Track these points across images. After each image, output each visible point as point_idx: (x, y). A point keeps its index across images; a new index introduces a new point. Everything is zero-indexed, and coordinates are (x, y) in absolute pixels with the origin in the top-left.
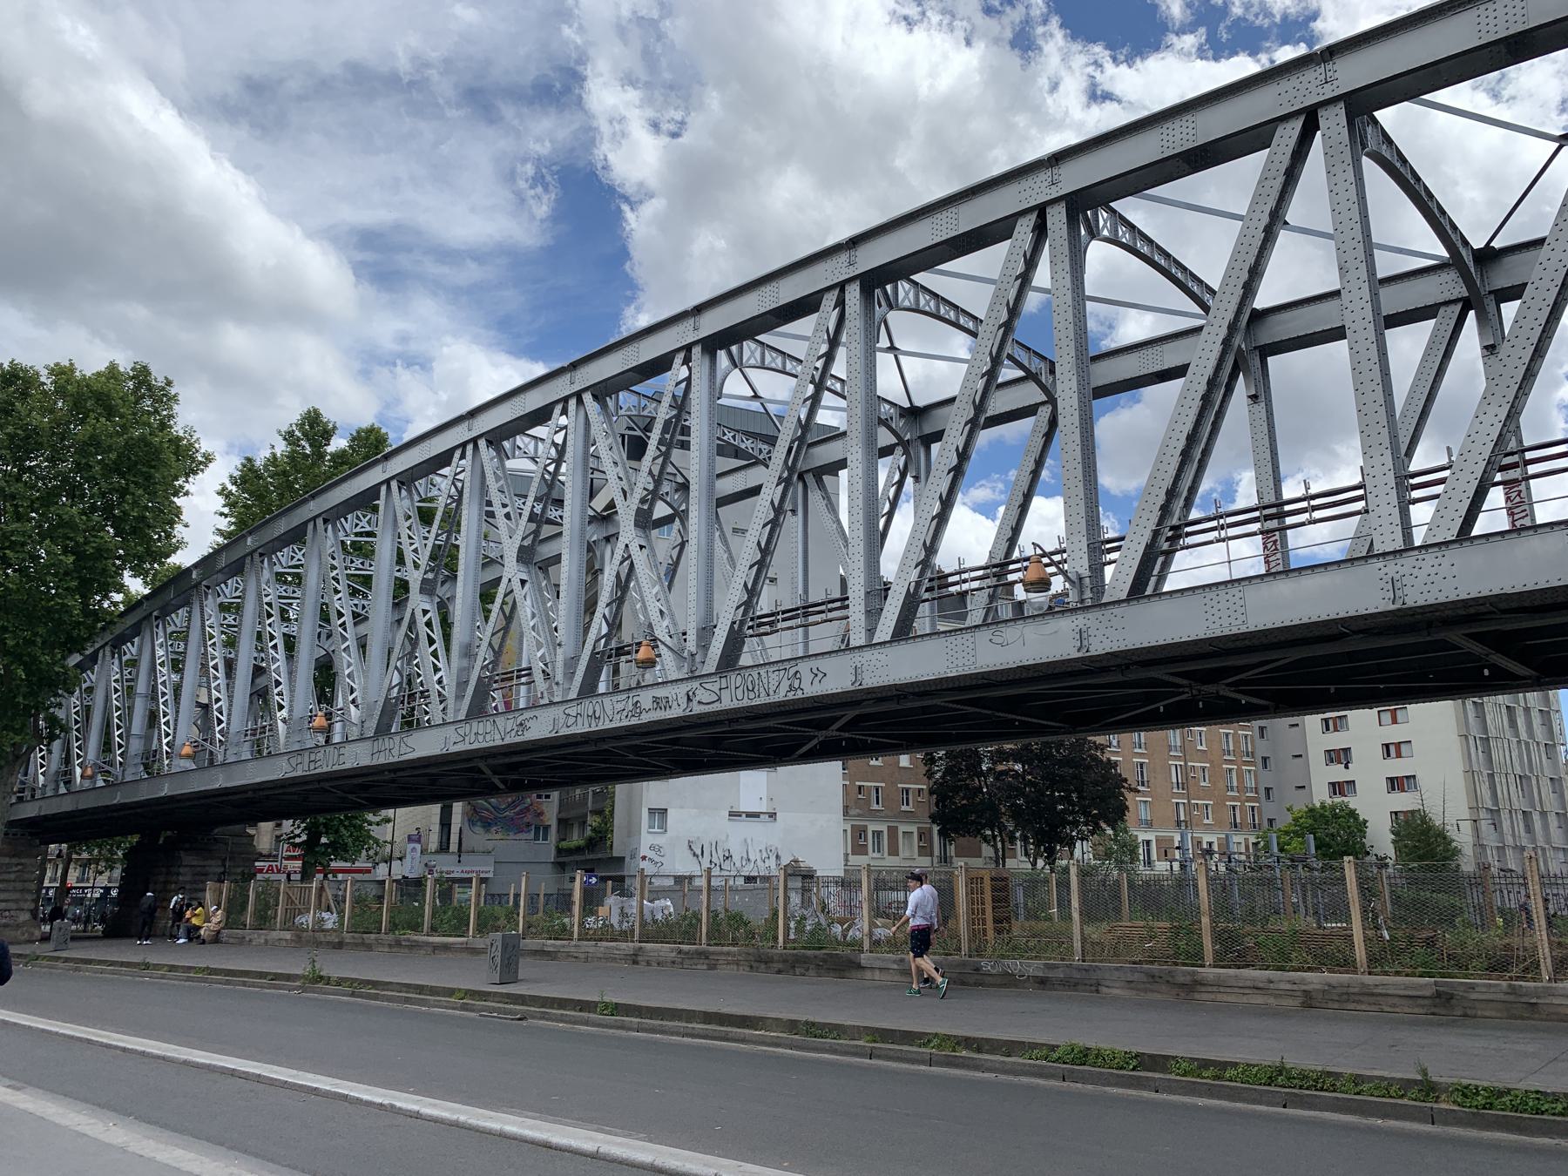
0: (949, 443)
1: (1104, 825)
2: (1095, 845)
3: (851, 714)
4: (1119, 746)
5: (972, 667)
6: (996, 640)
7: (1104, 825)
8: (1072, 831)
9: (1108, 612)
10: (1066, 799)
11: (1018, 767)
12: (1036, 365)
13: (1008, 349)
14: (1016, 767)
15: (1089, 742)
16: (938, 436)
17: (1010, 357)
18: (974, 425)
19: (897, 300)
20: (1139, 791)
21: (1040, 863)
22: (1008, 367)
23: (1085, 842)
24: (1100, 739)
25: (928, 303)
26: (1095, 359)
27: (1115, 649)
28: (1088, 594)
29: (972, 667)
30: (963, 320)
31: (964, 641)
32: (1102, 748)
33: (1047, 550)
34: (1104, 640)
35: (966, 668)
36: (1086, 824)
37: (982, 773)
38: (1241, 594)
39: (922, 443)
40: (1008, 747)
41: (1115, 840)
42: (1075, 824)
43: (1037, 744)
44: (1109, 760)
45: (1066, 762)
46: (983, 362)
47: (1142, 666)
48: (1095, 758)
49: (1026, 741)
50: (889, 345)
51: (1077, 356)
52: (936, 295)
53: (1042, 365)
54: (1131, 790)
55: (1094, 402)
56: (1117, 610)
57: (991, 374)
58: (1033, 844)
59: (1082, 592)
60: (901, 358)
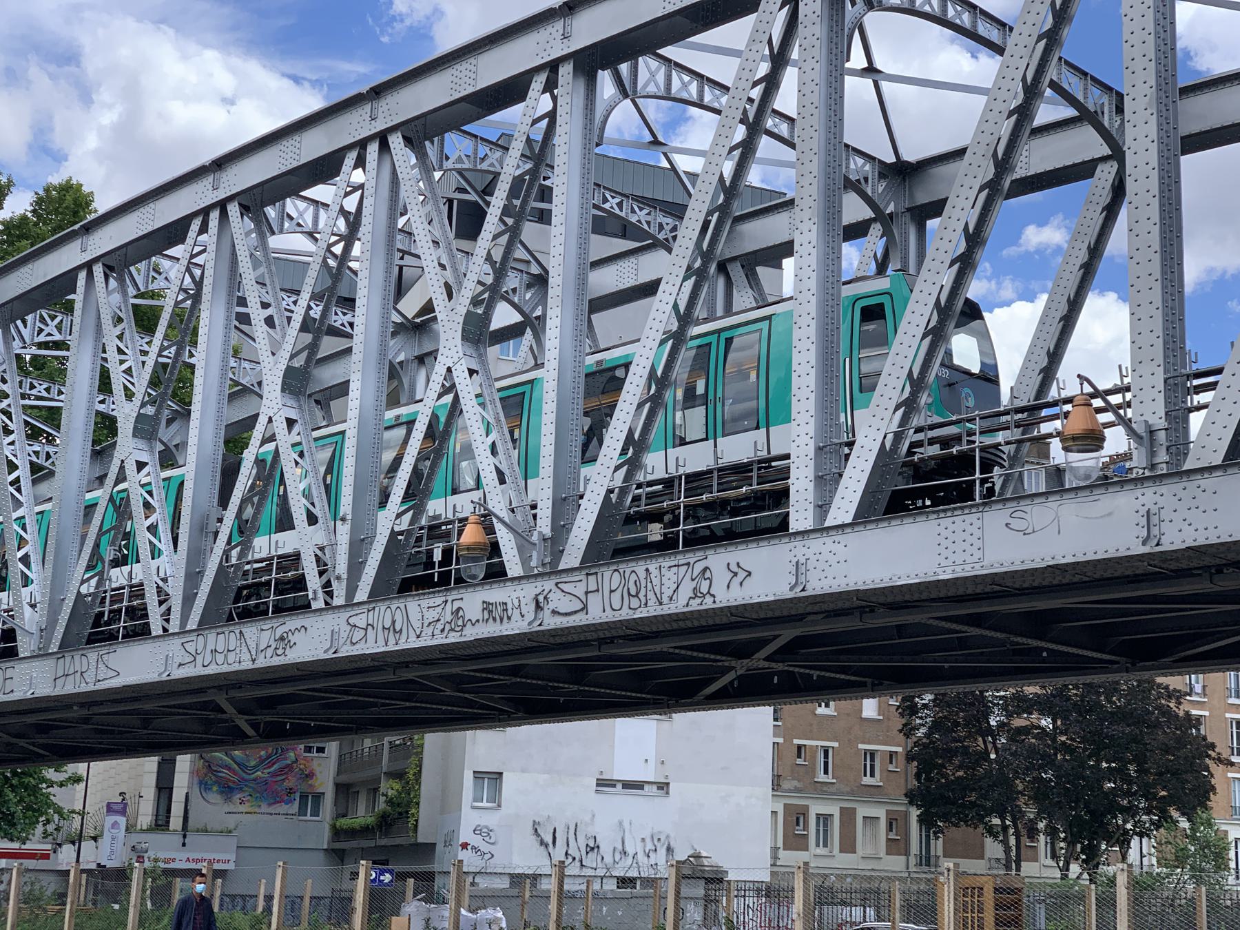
0: (954, 218)
1: (1175, 814)
2: (1160, 844)
4: (1205, 695)
5: (977, 566)
6: (1015, 524)
7: (1175, 814)
8: (1125, 822)
9: (1192, 485)
10: (1120, 774)
11: (1046, 722)
12: (1094, 99)
13: (1052, 73)
14: (1043, 723)
15: (1159, 685)
16: (936, 209)
17: (1053, 85)
18: (993, 189)
20: (1232, 764)
21: (1075, 869)
22: (1050, 102)
23: (1145, 840)
24: (1174, 682)
25: (685, 86)
26: (1186, 91)
27: (1201, 541)
28: (1162, 456)
29: (977, 566)
30: (984, 29)
31: (966, 525)
32: (1178, 696)
33: (1101, 387)
34: (1185, 526)
35: (968, 568)
36: (1148, 812)
37: (989, 731)
39: (913, 218)
40: (1031, 690)
41: (1193, 838)
42: (1130, 811)
43: (1076, 687)
44: (1187, 714)
45: (1122, 716)
46: (1012, 93)
47: (891, 609)
48: (1166, 712)
49: (1059, 681)
50: (866, 65)
51: (1158, 84)
52: (700, 76)
53: (1105, 99)
54: (1219, 760)
55: (1183, 158)
56: (1206, 482)
57: (1023, 113)
58: (1064, 840)
59: (1152, 453)
60: (884, 85)
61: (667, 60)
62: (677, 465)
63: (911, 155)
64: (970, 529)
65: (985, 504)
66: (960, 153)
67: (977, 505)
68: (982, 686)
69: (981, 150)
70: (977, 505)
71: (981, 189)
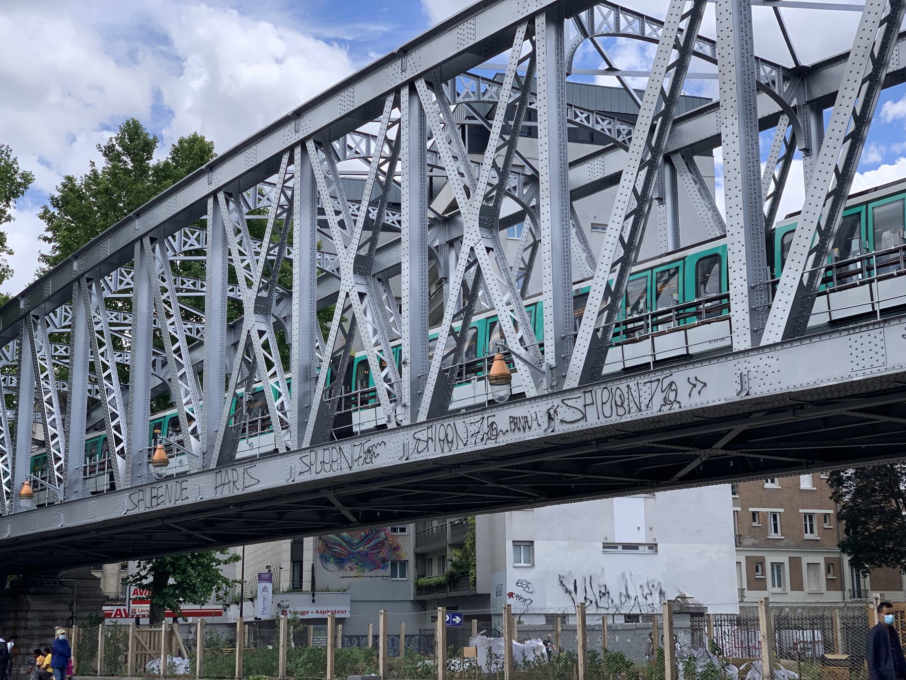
0: (844, 105)
3: (739, 428)
5: (882, 369)
16: (830, 99)
18: (872, 81)
19: (593, 26)
29: (882, 369)
31: (871, 338)
35: (875, 370)
38: (882, 336)
39: (812, 109)
60: (782, 10)
61: (367, 135)
62: (484, 353)
63: (807, 61)
64: (874, 341)
65: (884, 321)
66: (845, 56)
67: (879, 323)
68: (892, 460)
69: (861, 51)
70: (879, 323)
71: (863, 82)
